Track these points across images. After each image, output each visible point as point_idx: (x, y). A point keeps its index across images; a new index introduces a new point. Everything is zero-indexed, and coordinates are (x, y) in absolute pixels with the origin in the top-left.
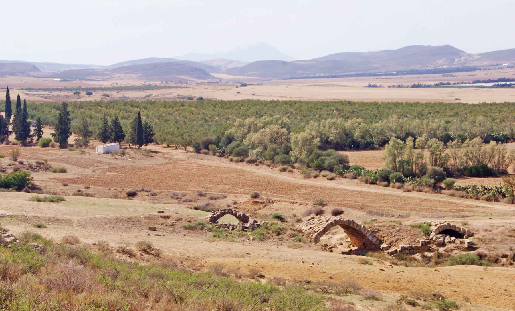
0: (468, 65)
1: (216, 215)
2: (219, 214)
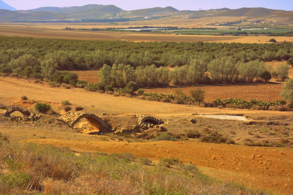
0: (124, 17)
1: (9, 111)
2: (11, 110)
